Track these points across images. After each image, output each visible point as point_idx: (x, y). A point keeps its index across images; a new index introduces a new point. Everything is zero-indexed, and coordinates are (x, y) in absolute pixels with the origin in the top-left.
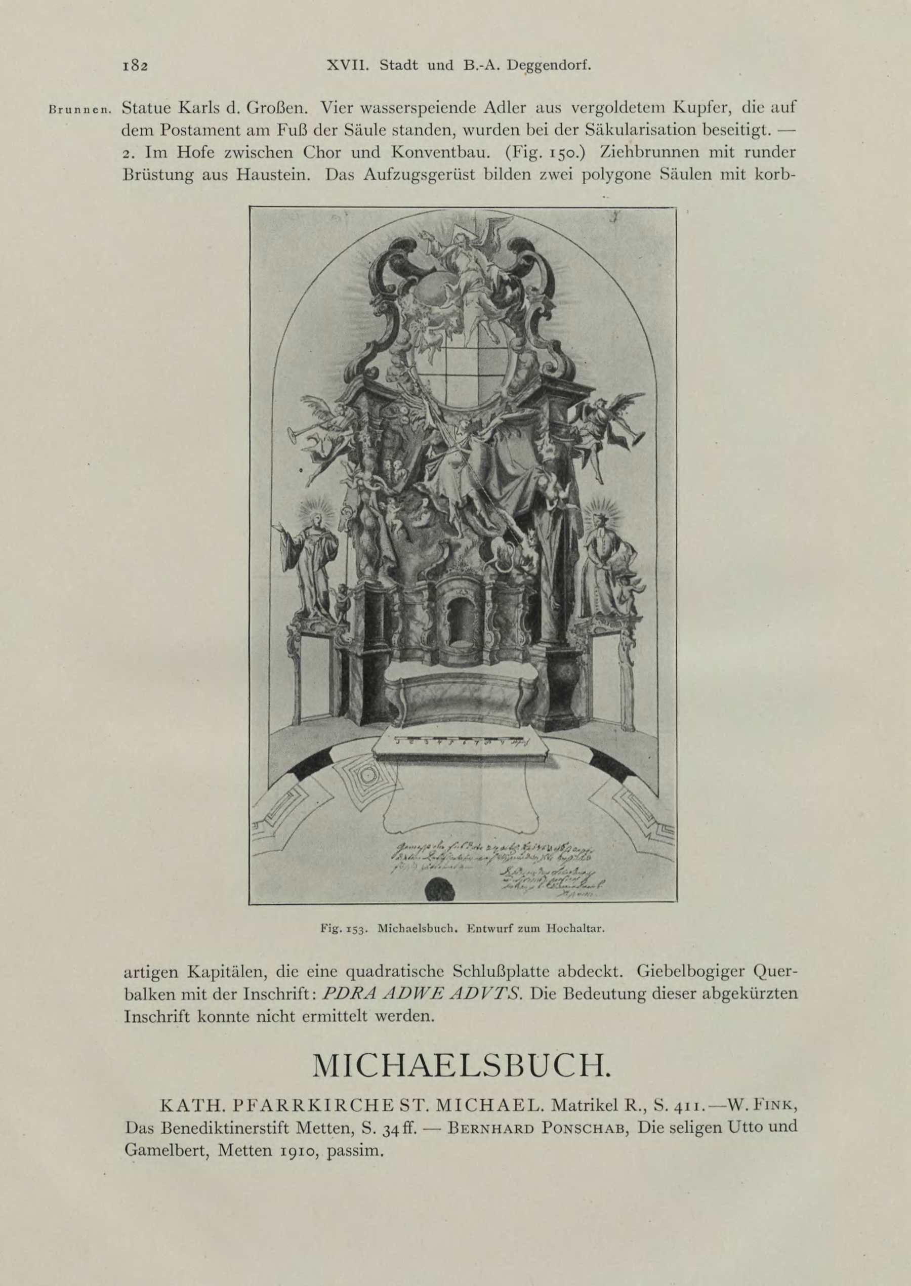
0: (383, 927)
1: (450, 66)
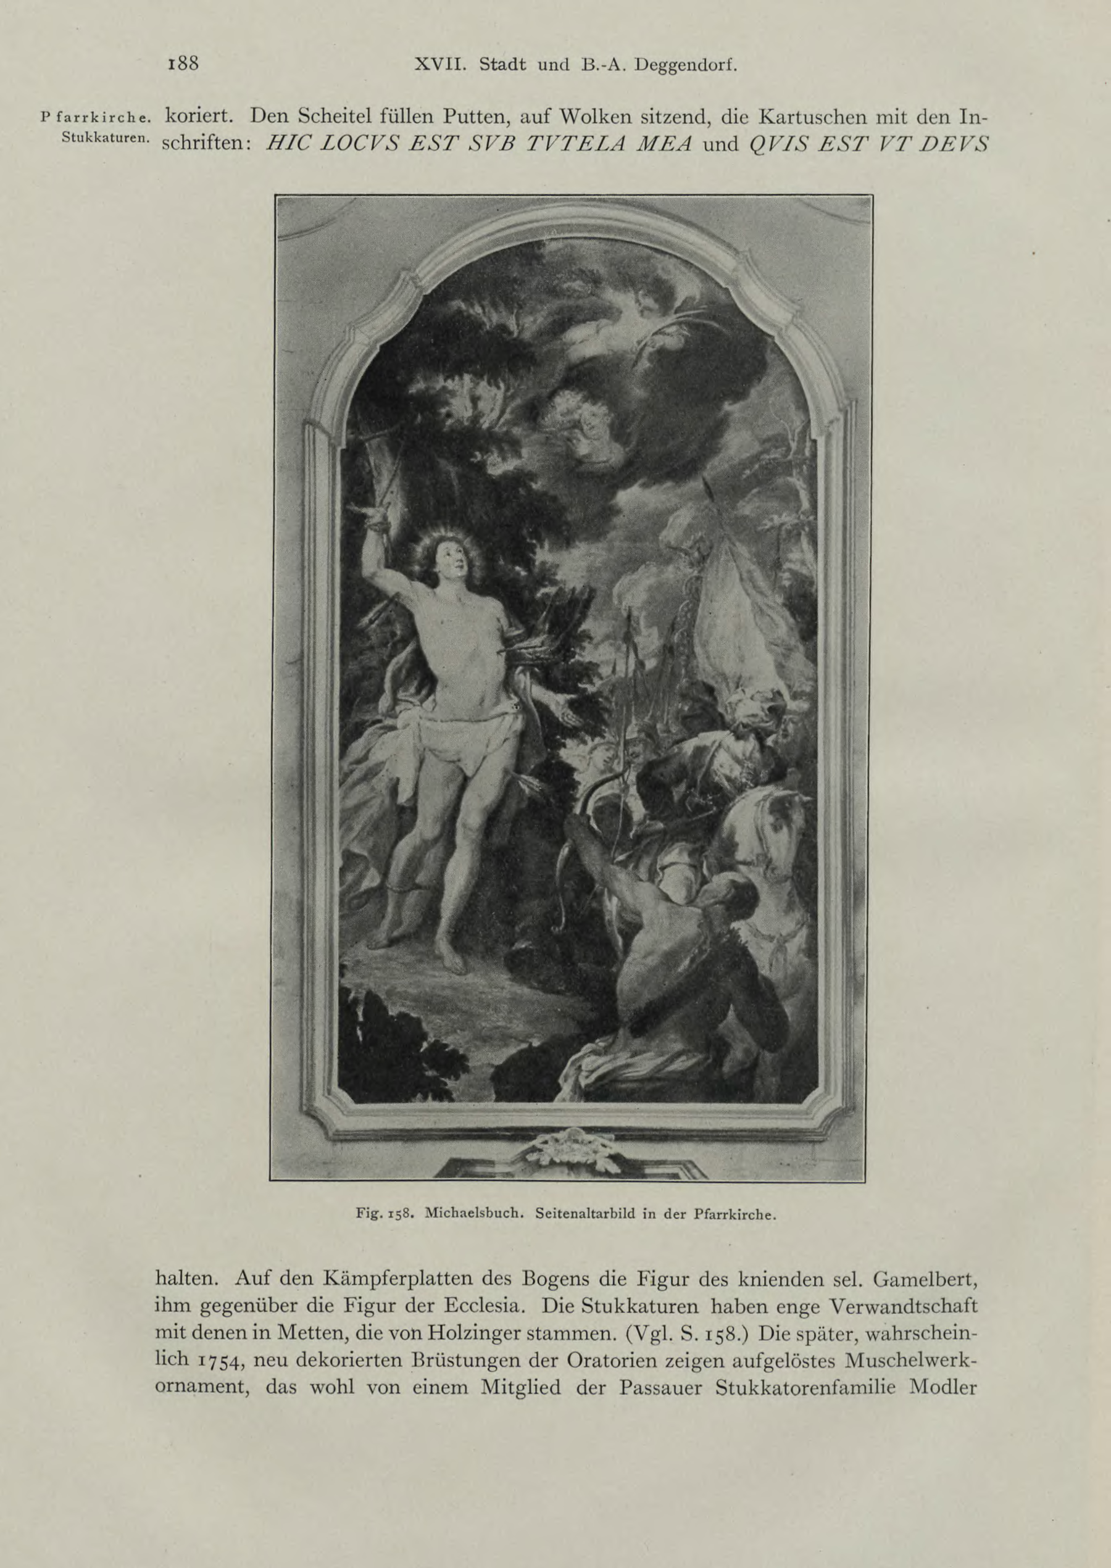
1: (566, 65)
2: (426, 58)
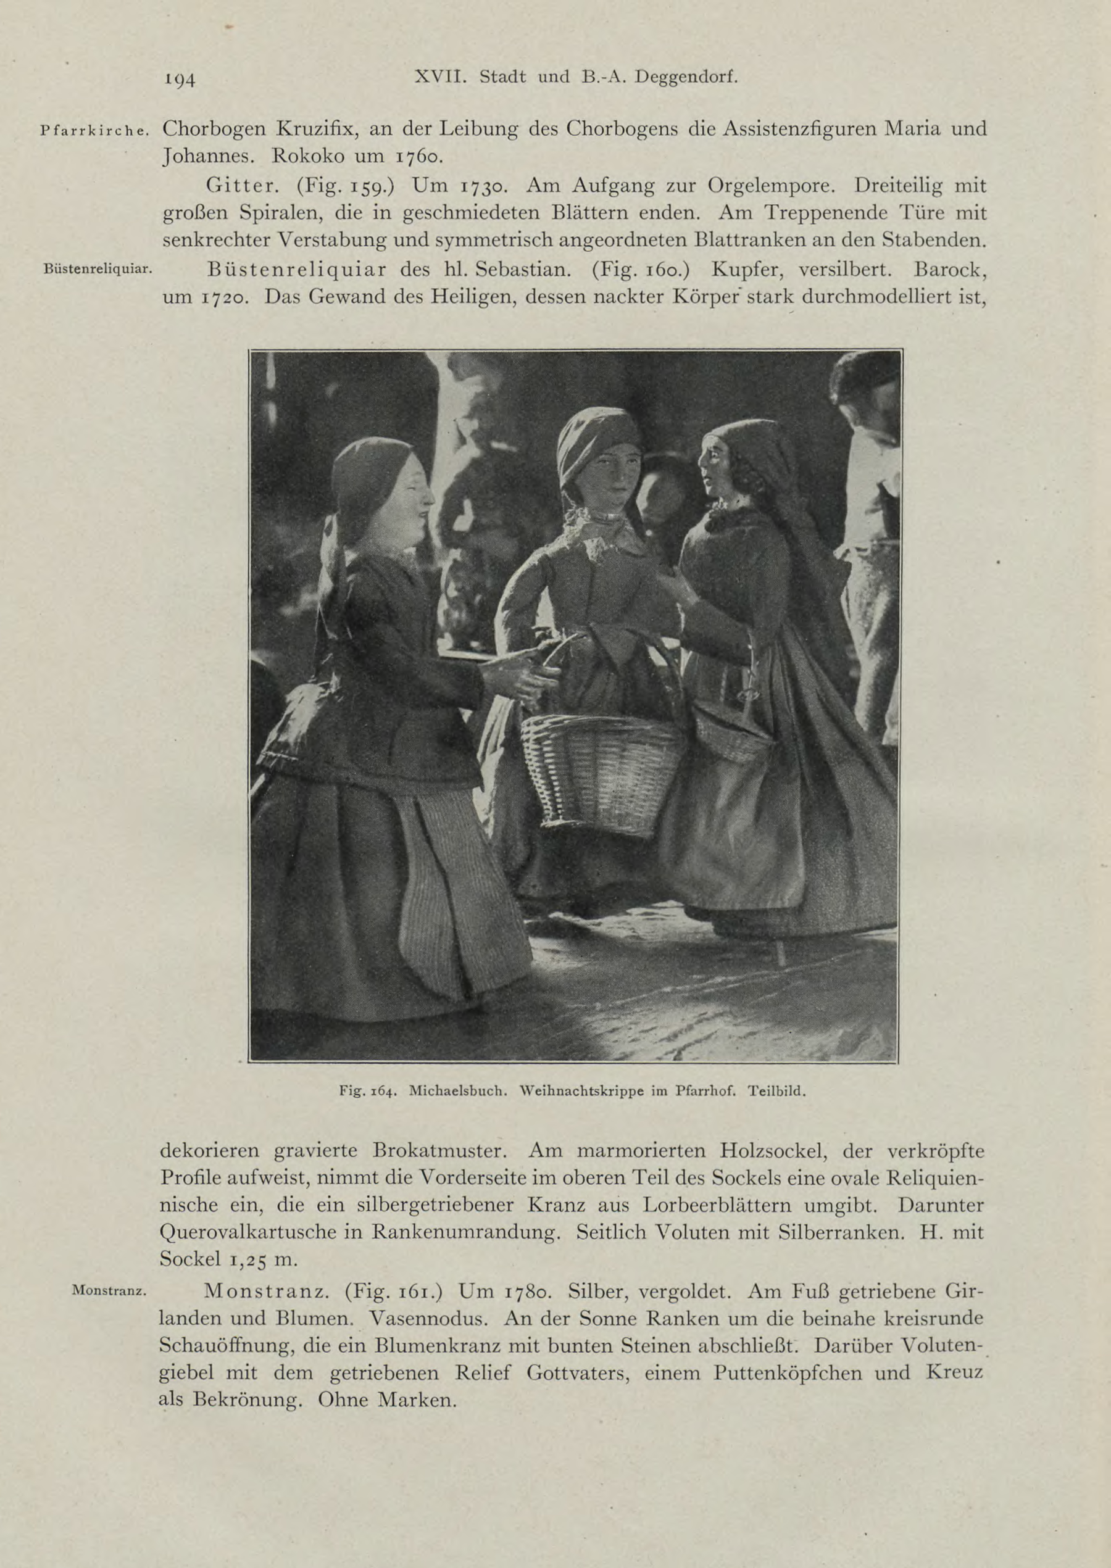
0: (416, 1088)
2: (426, 71)
